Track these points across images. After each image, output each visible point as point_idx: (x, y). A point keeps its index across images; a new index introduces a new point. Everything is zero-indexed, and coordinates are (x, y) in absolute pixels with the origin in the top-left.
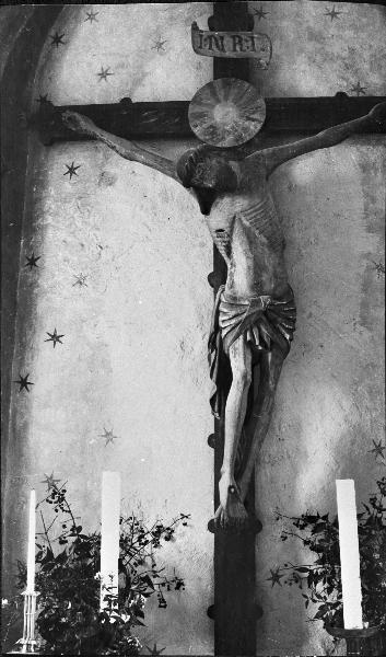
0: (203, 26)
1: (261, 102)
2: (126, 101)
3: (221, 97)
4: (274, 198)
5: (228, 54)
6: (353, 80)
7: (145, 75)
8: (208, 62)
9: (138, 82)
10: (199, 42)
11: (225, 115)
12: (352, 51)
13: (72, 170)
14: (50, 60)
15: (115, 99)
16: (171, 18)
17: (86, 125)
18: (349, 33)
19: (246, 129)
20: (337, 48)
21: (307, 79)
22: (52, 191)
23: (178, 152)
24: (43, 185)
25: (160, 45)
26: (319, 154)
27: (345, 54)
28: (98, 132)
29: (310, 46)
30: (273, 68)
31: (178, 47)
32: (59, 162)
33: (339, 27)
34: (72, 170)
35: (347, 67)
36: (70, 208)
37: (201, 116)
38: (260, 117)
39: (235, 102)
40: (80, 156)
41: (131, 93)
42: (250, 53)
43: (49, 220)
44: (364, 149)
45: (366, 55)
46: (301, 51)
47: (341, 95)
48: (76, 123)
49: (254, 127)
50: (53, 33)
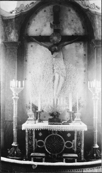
0: (52, 23)
1: (61, 36)
2: (40, 35)
3: (55, 35)
4: (63, 55)
5: (56, 28)
6: (75, 32)
7: (43, 30)
8: (53, 30)
9: (42, 31)
10: (52, 26)
11: (55, 38)
12: (75, 27)
13: (32, 46)
14: (28, 27)
15: (38, 35)
16: (47, 21)
17: (34, 39)
18: (75, 24)
19: (58, 41)
20: (73, 27)
21: (68, 32)
22: (29, 49)
23: (49, 44)
24: (27, 48)
25: (45, 25)
26: (69, 45)
27: (74, 28)
28: (36, 41)
29: (69, 26)
30: (63, 29)
31: (48, 26)
32: (29, 45)
33: (73, 23)
34: (32, 46)
35: (74, 30)
36: (32, 52)
37: (52, 38)
38: (60, 39)
39: (57, 36)
40: (33, 44)
41: (41, 34)
42: (59, 28)
43: (29, 54)
44: (66, 23)
45: (77, 28)
46: (68, 27)
47: (73, 35)
48: (33, 39)
49: (60, 40)
50: (28, 23)
